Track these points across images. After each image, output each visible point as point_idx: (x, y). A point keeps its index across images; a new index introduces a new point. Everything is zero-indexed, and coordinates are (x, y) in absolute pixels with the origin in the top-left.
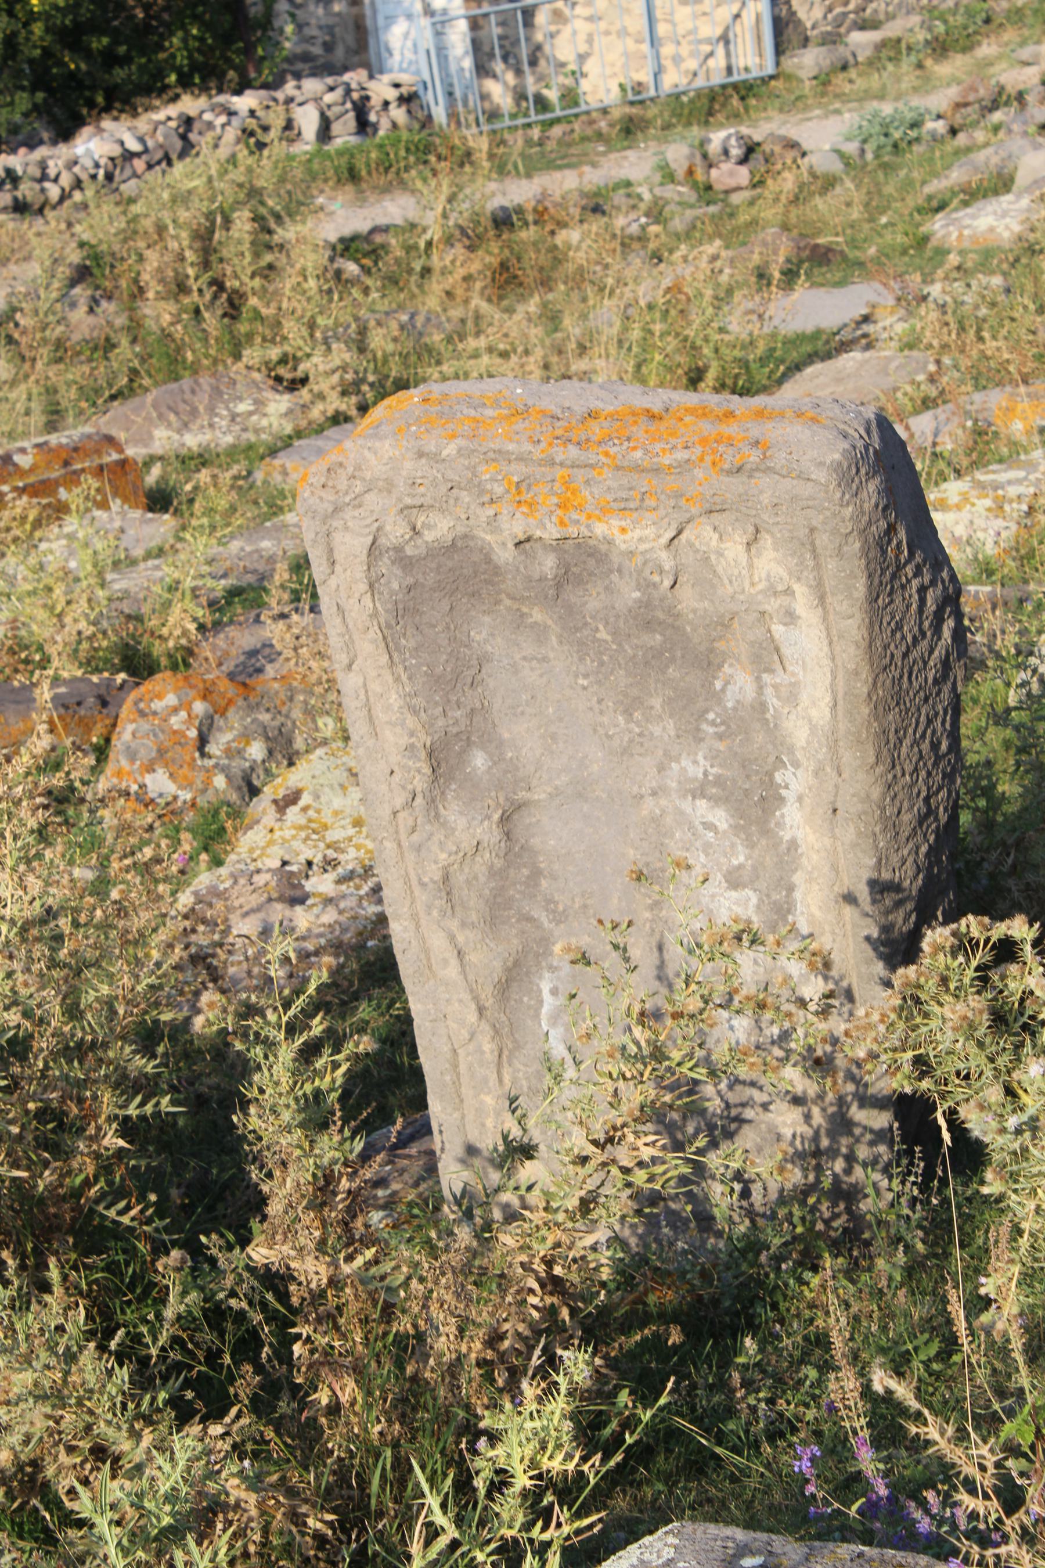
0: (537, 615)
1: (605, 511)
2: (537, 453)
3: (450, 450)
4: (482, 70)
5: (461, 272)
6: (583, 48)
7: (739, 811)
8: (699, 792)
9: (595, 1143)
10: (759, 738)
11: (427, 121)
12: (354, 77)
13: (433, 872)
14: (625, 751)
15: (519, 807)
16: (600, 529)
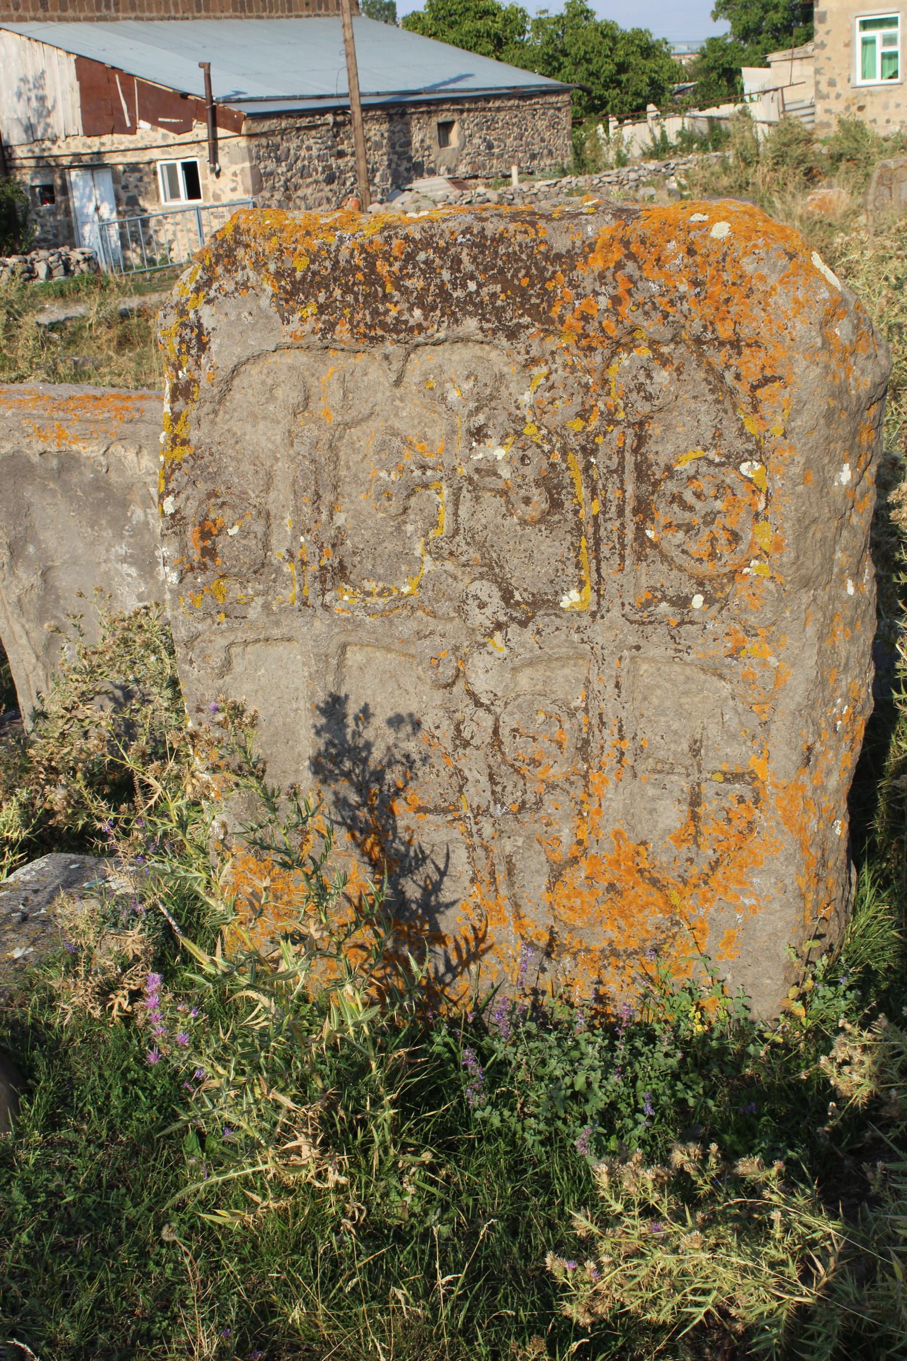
0: (52, 485)
1: (76, 440)
2: (46, 414)
3: (9, 414)
4: (125, 246)
5: (105, 338)
6: (171, 237)
7: (141, 569)
8: (124, 560)
9: (66, 709)
10: (147, 537)
11: (97, 270)
12: (63, 250)
13: (13, 598)
14: (92, 544)
15: (49, 569)
16: (74, 447)
